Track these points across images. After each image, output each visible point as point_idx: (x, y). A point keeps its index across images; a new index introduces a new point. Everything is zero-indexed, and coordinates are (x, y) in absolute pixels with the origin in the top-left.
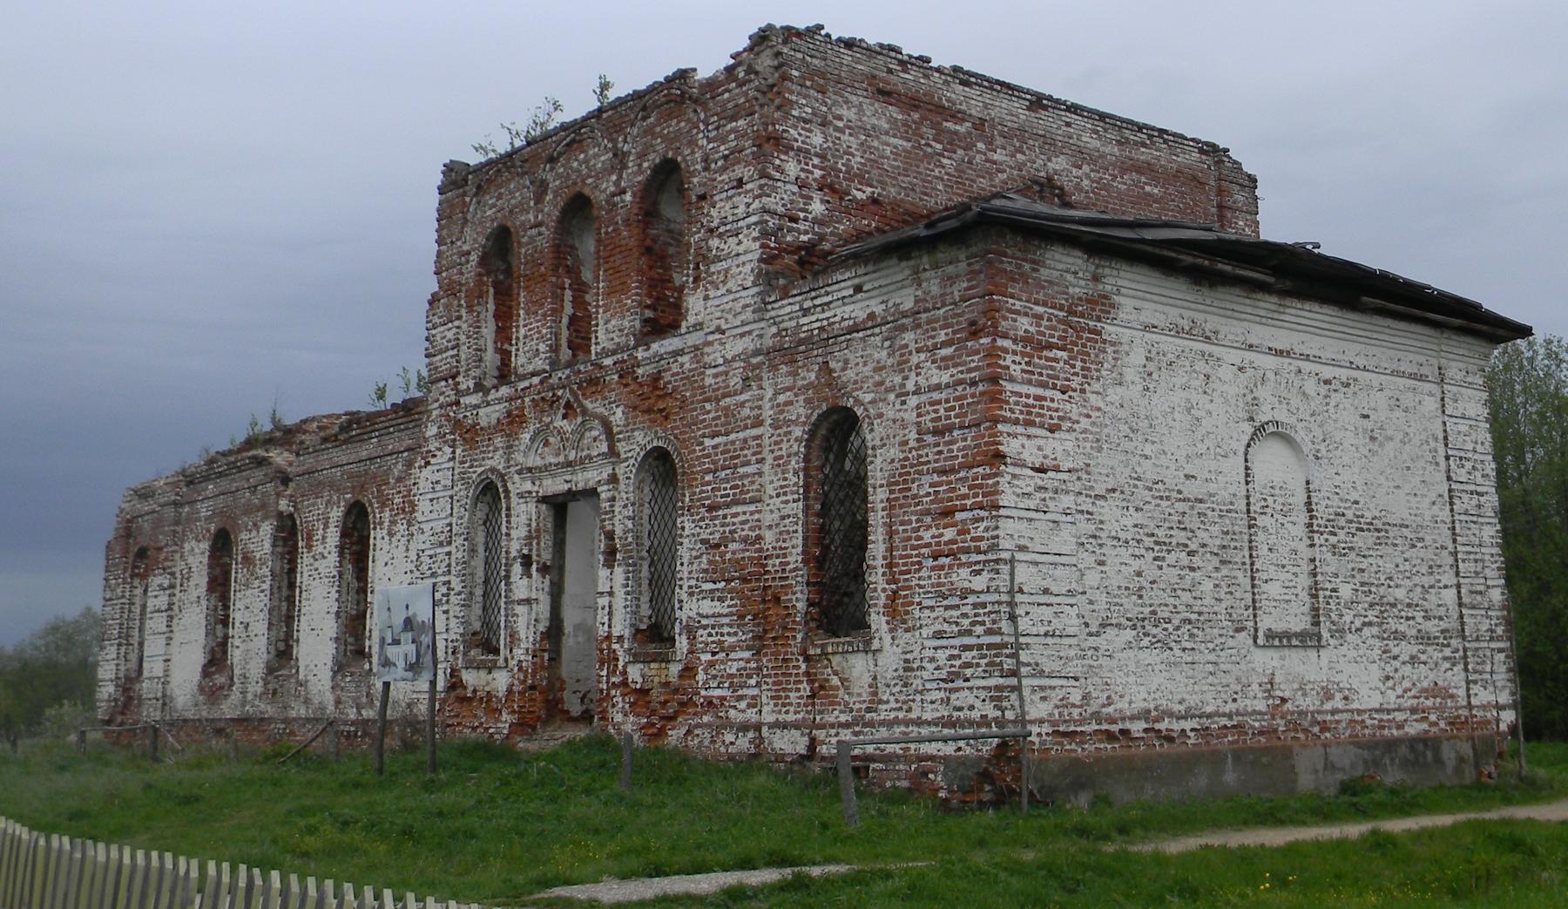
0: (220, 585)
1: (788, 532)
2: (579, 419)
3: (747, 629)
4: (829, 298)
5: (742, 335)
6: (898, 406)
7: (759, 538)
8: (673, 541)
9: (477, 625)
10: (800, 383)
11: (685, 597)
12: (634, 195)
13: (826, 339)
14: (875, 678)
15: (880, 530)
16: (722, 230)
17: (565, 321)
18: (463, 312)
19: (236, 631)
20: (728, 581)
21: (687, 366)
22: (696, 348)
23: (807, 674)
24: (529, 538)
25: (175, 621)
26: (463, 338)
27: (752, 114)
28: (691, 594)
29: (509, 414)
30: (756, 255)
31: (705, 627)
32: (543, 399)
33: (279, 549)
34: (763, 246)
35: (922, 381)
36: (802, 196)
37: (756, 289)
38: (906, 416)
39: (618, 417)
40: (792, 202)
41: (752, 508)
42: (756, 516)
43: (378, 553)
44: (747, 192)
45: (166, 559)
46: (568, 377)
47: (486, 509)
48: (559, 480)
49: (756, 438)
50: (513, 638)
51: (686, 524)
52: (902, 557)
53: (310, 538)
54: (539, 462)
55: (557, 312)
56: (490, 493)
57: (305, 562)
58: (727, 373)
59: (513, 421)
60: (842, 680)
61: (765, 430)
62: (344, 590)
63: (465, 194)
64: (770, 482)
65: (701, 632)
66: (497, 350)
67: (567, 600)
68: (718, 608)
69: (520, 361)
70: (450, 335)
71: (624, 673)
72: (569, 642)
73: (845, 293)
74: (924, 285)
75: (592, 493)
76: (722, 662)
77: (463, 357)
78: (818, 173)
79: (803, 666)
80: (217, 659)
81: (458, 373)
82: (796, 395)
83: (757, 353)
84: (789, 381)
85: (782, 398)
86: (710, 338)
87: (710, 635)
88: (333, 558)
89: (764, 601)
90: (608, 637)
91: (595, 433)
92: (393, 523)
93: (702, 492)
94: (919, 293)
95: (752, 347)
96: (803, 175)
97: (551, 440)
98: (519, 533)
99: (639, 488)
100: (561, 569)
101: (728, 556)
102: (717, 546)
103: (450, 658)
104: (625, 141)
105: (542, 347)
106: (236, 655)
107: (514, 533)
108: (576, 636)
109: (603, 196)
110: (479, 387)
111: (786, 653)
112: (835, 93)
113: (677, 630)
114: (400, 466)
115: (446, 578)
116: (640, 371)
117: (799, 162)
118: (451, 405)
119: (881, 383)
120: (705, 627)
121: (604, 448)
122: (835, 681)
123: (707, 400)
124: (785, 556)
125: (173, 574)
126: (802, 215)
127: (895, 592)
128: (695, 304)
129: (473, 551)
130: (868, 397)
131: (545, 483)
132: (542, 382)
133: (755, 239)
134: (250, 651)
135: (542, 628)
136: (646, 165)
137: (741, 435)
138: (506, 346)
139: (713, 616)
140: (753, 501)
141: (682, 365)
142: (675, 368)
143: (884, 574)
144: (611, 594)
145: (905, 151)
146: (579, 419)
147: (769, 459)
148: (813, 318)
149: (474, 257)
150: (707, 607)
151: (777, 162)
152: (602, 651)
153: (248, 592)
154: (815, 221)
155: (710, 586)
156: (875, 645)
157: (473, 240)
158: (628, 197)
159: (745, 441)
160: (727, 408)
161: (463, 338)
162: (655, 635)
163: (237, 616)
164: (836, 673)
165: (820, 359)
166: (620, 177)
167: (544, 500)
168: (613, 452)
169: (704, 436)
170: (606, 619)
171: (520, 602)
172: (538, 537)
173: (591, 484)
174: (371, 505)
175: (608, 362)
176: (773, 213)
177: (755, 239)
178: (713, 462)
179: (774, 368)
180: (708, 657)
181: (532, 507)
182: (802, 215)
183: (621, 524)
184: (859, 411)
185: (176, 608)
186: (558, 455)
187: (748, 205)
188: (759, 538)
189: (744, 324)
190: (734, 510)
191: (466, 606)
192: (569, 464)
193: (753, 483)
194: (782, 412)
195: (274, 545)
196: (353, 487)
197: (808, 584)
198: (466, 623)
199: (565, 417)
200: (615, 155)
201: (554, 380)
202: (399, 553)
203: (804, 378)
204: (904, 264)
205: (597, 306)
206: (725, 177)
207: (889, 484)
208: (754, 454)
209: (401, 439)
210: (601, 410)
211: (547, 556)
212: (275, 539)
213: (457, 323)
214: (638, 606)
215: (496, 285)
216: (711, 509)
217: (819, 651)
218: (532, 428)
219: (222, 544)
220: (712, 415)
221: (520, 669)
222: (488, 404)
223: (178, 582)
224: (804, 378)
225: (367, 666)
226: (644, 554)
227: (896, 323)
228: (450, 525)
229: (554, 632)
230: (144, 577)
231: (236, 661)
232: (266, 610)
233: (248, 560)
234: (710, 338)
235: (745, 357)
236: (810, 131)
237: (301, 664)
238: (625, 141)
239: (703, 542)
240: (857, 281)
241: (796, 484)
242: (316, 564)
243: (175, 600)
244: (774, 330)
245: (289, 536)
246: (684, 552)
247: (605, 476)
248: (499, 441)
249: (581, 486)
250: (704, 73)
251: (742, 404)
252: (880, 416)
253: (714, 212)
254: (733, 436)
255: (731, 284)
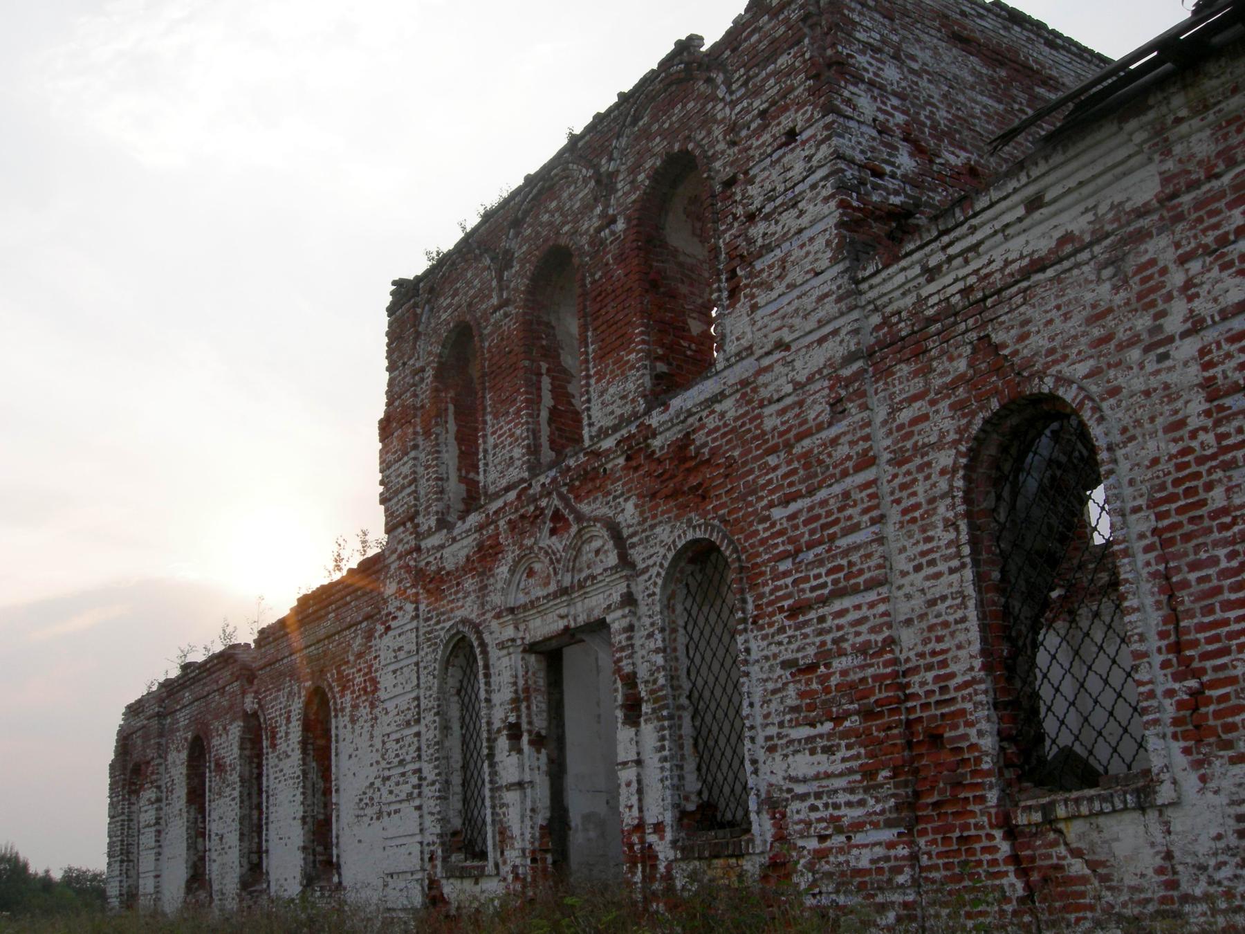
0: (197, 797)
1: (946, 624)
2: (574, 529)
3: (883, 792)
4: (979, 236)
5: (821, 341)
6: (1150, 367)
7: (891, 641)
8: (732, 667)
9: (457, 823)
10: (937, 382)
11: (761, 755)
12: (628, 220)
13: (980, 301)
14: (1169, 856)
15: (1146, 587)
16: (767, 210)
17: (544, 414)
18: (420, 440)
19: (213, 844)
20: (838, 720)
21: (731, 414)
22: (744, 383)
23: (1014, 859)
24: (516, 701)
25: (163, 835)
26: (421, 470)
27: (799, 42)
28: (772, 749)
29: (480, 547)
30: (832, 221)
31: (803, 797)
32: (523, 517)
33: (247, 752)
34: (843, 205)
35: (1202, 306)
36: (886, 145)
37: (840, 267)
38: (1172, 378)
39: (628, 513)
40: (873, 149)
41: (872, 596)
42: (882, 608)
43: (341, 745)
44: (804, 143)
45: (152, 773)
46: (554, 480)
47: (459, 675)
48: (552, 617)
49: (867, 485)
50: (504, 836)
51: (753, 645)
52: (1202, 628)
53: (274, 737)
54: (523, 599)
55: (534, 403)
56: (463, 653)
57: (270, 760)
58: (801, 404)
59: (487, 554)
60: (1093, 865)
61: (882, 471)
62: (309, 792)
63: (416, 305)
64: (902, 548)
65: (796, 805)
66: (462, 479)
67: (570, 780)
68: (823, 763)
69: (491, 476)
70: (406, 470)
71: (669, 877)
72: (579, 839)
73: (1009, 218)
74: (1178, 149)
75: (599, 627)
76: (841, 850)
77: (422, 493)
78: (900, 118)
79: (1005, 848)
80: (197, 878)
81: (417, 513)
82: (933, 403)
83: (850, 358)
84: (917, 384)
85: (905, 416)
86: (766, 362)
87: (813, 808)
88: (297, 755)
89: (910, 745)
90: (640, 827)
91: (596, 544)
92: (355, 707)
93: (777, 588)
94: (1170, 165)
95: (841, 352)
96: (881, 117)
97: (537, 567)
98: (503, 695)
99: (668, 606)
100: (561, 741)
101: (834, 681)
102: (812, 668)
103: (428, 866)
104: (611, 159)
105: (517, 452)
106: (214, 870)
107: (496, 698)
108: (586, 830)
109: (584, 240)
110: (443, 524)
111: (966, 827)
112: (904, 27)
113: (752, 806)
114: (359, 641)
115: (417, 766)
116: (656, 443)
117: (874, 99)
118: (410, 552)
119: (1107, 339)
120: (803, 797)
121: (612, 559)
122: (1077, 867)
123: (773, 450)
124: (944, 664)
125: (159, 787)
126: (888, 169)
127: (1195, 694)
128: (736, 326)
129: (445, 728)
130: (1082, 369)
131: (531, 625)
132: (519, 497)
133: (826, 200)
134: (226, 867)
135: (541, 819)
136: (641, 177)
137: (837, 489)
138: (472, 475)
139: (817, 777)
140: (871, 585)
141: (722, 415)
142: (711, 423)
143: (1165, 665)
144: (639, 762)
145: (997, 113)
146: (574, 529)
147: (894, 514)
148: (949, 279)
149: (430, 373)
150: (803, 764)
151: (846, 94)
152: (631, 846)
153: (223, 800)
154: (905, 179)
155: (806, 731)
156: (1165, 793)
157: (429, 352)
158: (620, 225)
159: (846, 495)
160: (807, 454)
161: (421, 470)
162: (711, 818)
163: (214, 827)
164: (1077, 853)
165: (973, 336)
166: (607, 206)
167: (531, 648)
168: (625, 561)
169: (771, 505)
170: (634, 800)
171: (509, 787)
172: (528, 699)
173: (597, 614)
174: (331, 688)
175: (608, 443)
176: (851, 161)
177: (826, 200)
178: (791, 541)
179: (884, 373)
180: (813, 844)
181: (516, 659)
182: (888, 169)
183: (647, 659)
184: (1069, 395)
185: (162, 822)
186: (547, 584)
187: (809, 158)
188: (891, 641)
189: (821, 324)
190: (837, 605)
191: (443, 798)
192: (564, 591)
193: (869, 556)
194: (909, 435)
195: (242, 748)
196: (313, 673)
197: (996, 706)
198: (444, 821)
199: (553, 532)
200: (598, 182)
201: (536, 488)
202: (363, 742)
203: (945, 373)
204: (1132, 124)
205: (588, 377)
206: (766, 137)
207: (1153, 504)
208: (866, 511)
209: (359, 608)
210: (605, 511)
211: (540, 723)
212: (242, 741)
213: (413, 454)
214: (681, 778)
215: (456, 402)
216: (794, 612)
217: (1037, 817)
218: (510, 557)
219: (198, 751)
220: (780, 472)
221: (516, 877)
222: (454, 540)
223: (164, 795)
224: (945, 373)
225: (336, 879)
226: (684, 701)
227: (1120, 240)
228: (417, 698)
229: (556, 828)
230: (137, 792)
231: (214, 876)
232: (237, 818)
233: (220, 767)
234: (766, 362)
235: (831, 372)
236: (883, 63)
237: (272, 877)
238: (611, 159)
239: (785, 665)
240: (1031, 190)
241: (955, 543)
242: (281, 765)
243: (162, 813)
244: (876, 319)
245: (256, 738)
246: (755, 683)
247: (616, 597)
248: (469, 583)
249: (581, 620)
250: (712, 35)
251: (834, 442)
252: (1114, 392)
253: (752, 190)
254: (822, 494)
255: (794, 275)
